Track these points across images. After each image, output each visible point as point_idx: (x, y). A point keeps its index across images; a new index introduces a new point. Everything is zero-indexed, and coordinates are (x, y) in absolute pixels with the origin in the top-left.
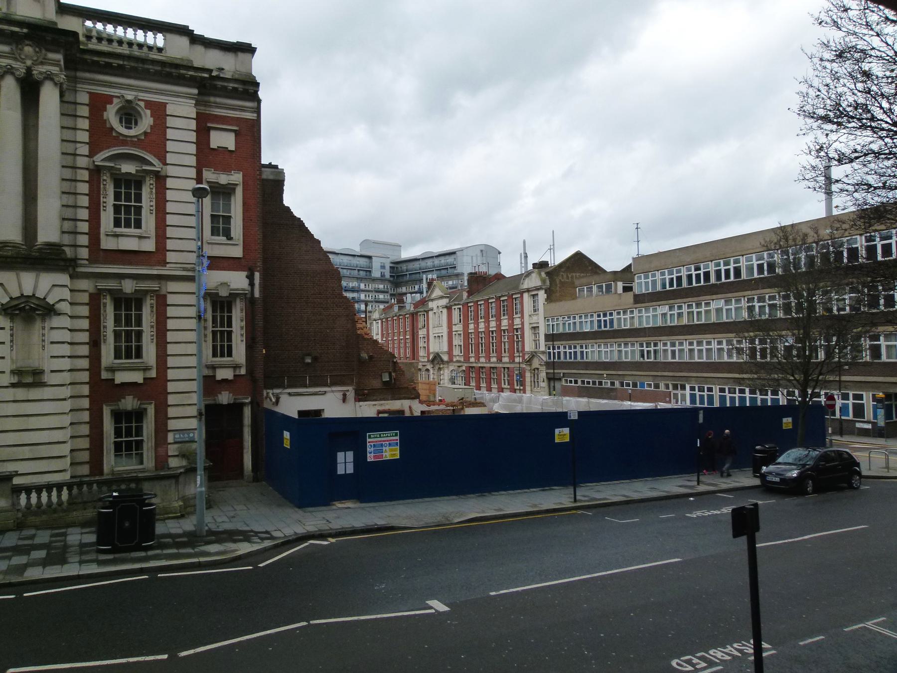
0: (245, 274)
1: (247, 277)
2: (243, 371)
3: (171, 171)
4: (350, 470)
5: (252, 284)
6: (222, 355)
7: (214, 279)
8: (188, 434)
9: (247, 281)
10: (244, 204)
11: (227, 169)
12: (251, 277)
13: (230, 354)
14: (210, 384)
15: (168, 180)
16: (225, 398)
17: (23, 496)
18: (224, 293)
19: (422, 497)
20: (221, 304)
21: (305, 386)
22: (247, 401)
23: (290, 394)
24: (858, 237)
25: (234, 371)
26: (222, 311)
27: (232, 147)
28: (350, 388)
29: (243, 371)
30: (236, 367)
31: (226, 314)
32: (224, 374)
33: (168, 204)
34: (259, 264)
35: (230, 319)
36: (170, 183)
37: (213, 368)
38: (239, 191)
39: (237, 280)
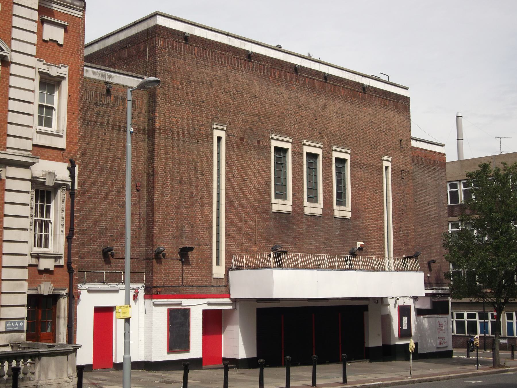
0: (65, 165)
1: (68, 168)
2: (62, 262)
3: (15, 57)
4: (406, 328)
5: (72, 176)
6: (40, 246)
7: (42, 168)
8: (19, 323)
9: (68, 172)
10: (69, 97)
11: (56, 63)
12: (71, 170)
13: (46, 246)
14: (37, 273)
15: (12, 66)
16: (46, 288)
17: (6, 363)
18: (49, 182)
19: (447, 357)
20: (43, 193)
21: (101, 282)
22: (64, 293)
23: (90, 291)
24: (458, 182)
25: (55, 261)
26: (42, 201)
27: (61, 42)
28: (140, 286)
29: (62, 262)
30: (56, 257)
31: (45, 204)
32: (46, 264)
33: (11, 90)
34: (78, 157)
35: (48, 208)
36: (13, 69)
37: (38, 256)
38: (65, 84)
39: (61, 171)
